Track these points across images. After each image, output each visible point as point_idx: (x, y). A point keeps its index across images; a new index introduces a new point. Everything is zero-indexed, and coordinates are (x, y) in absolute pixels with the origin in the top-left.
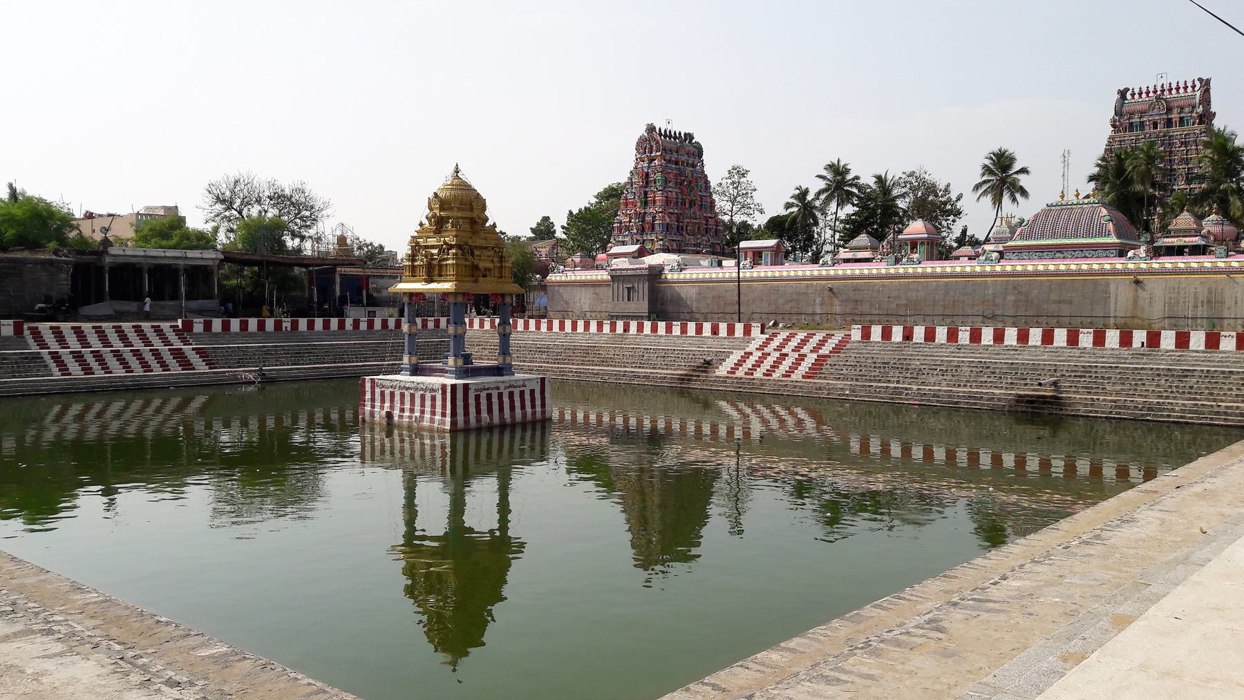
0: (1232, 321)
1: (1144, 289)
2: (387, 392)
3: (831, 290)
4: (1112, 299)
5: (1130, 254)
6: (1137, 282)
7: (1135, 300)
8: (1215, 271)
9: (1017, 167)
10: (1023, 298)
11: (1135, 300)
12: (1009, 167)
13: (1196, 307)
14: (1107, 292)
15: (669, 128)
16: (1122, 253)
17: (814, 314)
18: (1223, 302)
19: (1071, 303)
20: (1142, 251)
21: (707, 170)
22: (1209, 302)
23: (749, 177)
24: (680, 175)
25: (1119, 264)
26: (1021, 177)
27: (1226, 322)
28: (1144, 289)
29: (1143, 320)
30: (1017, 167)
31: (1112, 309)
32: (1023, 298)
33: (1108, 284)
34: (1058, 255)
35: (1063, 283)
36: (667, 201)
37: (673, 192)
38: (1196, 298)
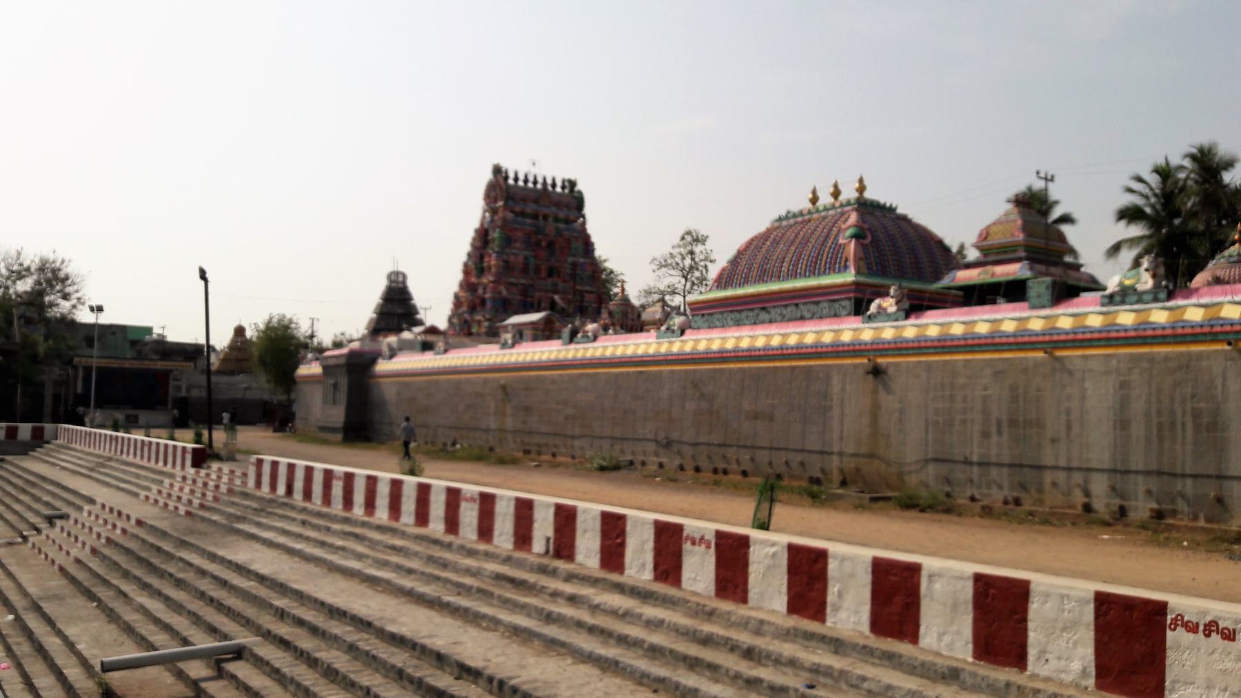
0: (1061, 476)
1: (888, 390)
2: (358, 511)
3: (504, 388)
4: (836, 412)
5: (873, 308)
6: (876, 372)
7: (875, 409)
8: (1023, 342)
9: (1056, 213)
10: (704, 405)
11: (875, 409)
12: (1045, 213)
13: (986, 435)
14: (826, 395)
15: (533, 171)
16: (860, 308)
17: (487, 430)
18: (1040, 424)
19: (771, 418)
20: (889, 304)
21: (591, 229)
22: (1013, 422)
23: (709, 245)
24: (537, 233)
25: (851, 330)
26: (1066, 229)
27: (1048, 477)
28: (888, 390)
29: (888, 464)
30: (1056, 213)
31: (836, 435)
32: (704, 405)
33: (828, 377)
34: (763, 316)
35: (758, 375)
36: (507, 267)
37: (519, 254)
38: (986, 412)
